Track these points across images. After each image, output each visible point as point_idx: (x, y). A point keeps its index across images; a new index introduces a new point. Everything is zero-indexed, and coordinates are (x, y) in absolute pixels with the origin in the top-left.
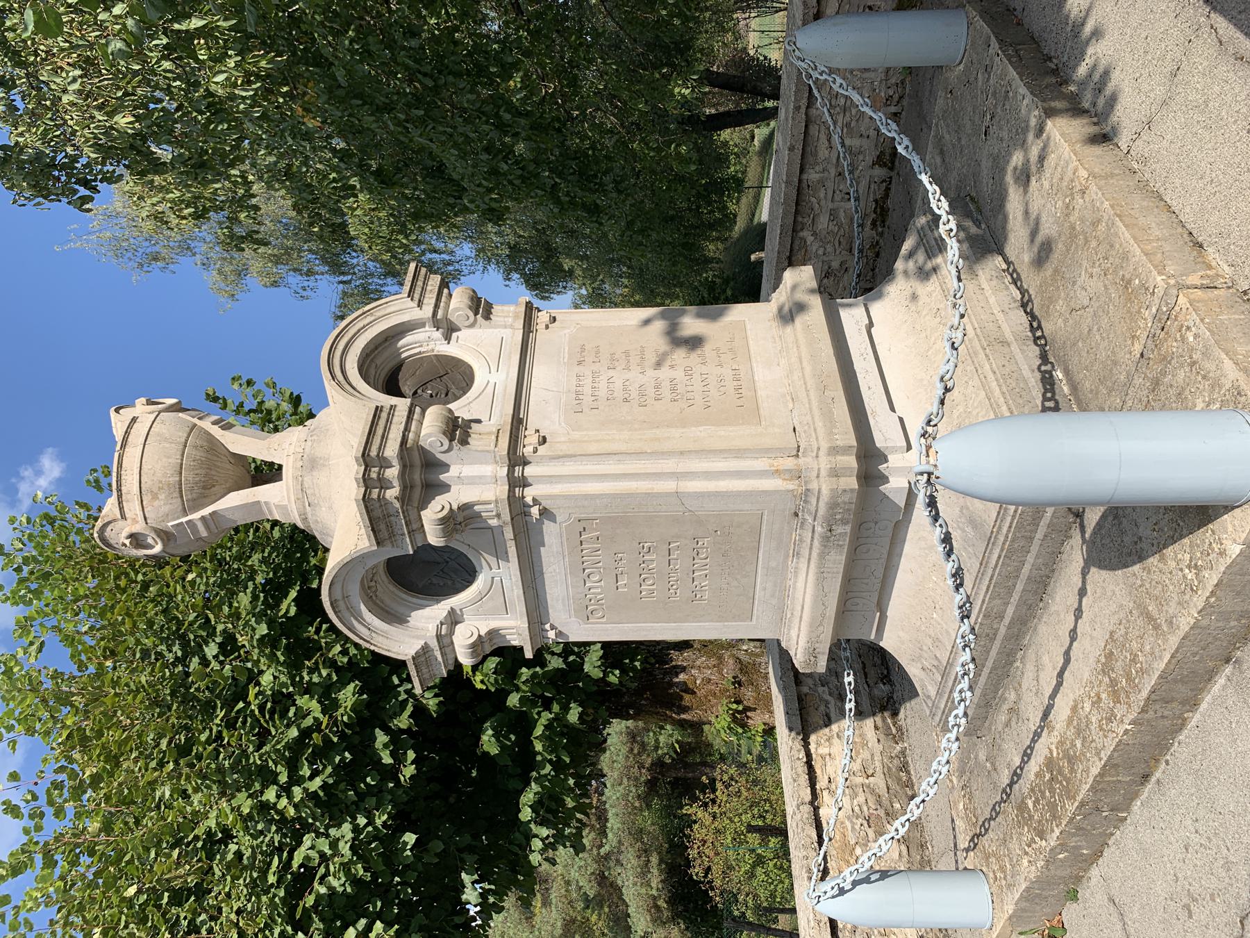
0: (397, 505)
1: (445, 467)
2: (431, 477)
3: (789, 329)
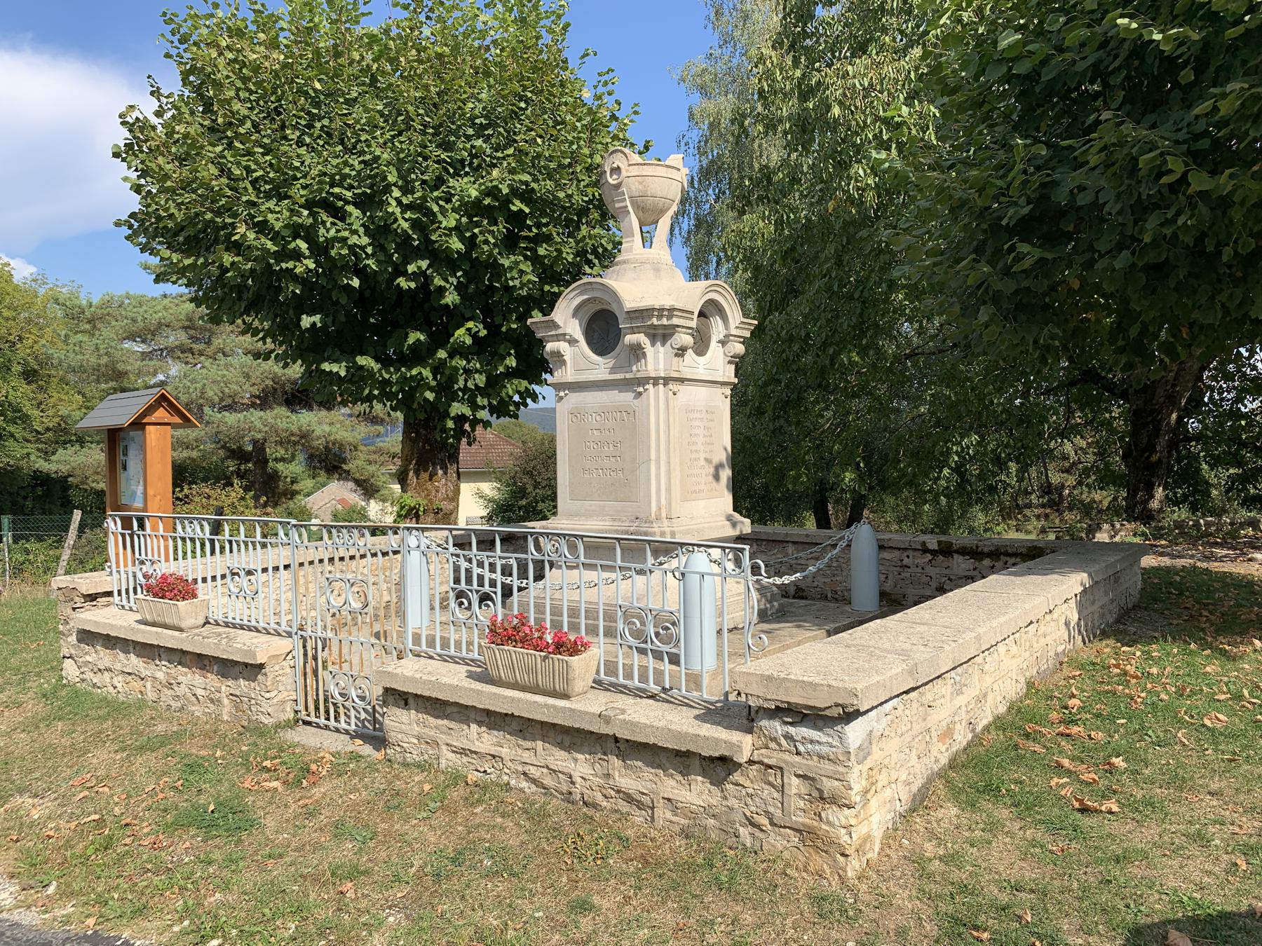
1: (663, 345)
2: (659, 338)
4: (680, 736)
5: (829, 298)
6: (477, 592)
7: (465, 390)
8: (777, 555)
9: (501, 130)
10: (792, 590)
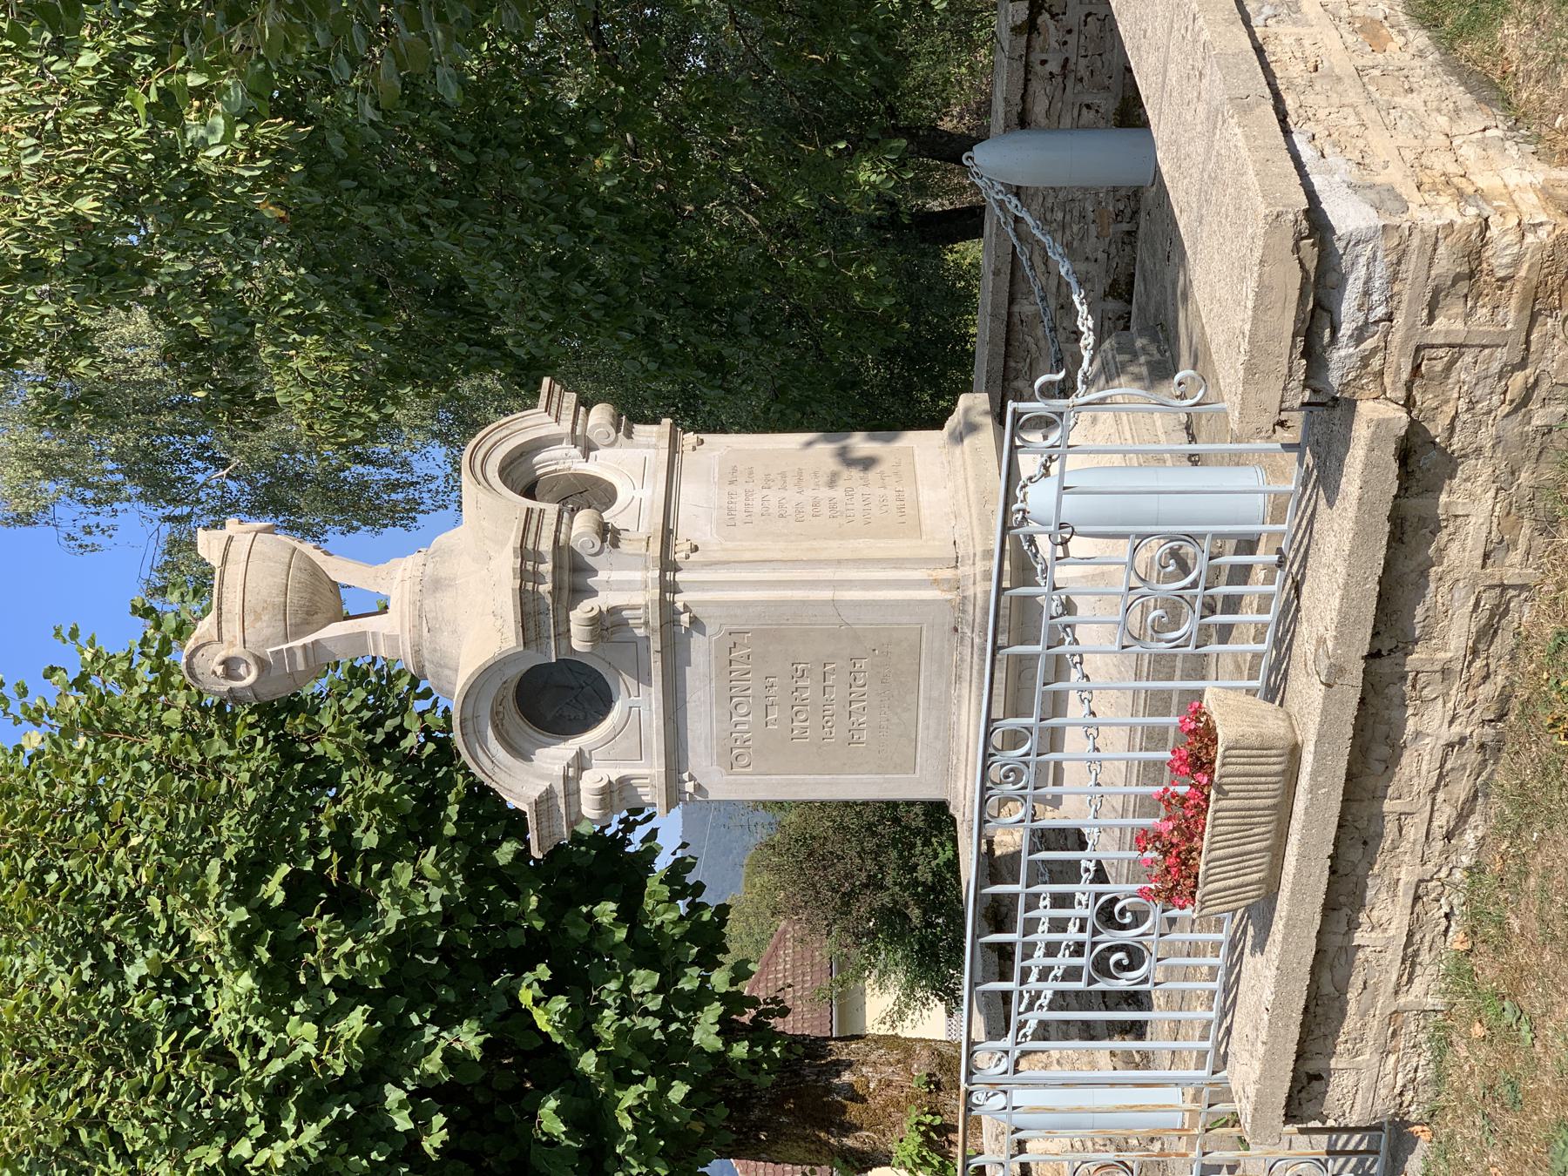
0: (549, 600)
1: (594, 572)
3: (958, 450)
4: (1362, 533)
5: (472, 216)
6: (1095, 932)
7: (665, 1016)
8: (1039, 337)
9: (107, 924)
10: (1113, 305)
